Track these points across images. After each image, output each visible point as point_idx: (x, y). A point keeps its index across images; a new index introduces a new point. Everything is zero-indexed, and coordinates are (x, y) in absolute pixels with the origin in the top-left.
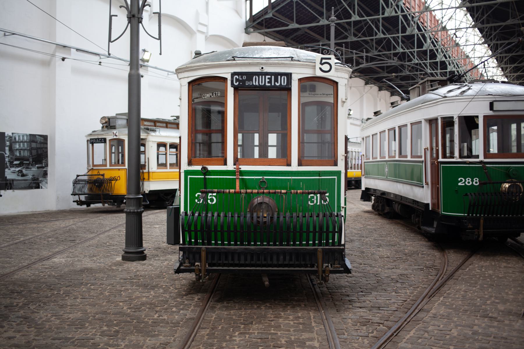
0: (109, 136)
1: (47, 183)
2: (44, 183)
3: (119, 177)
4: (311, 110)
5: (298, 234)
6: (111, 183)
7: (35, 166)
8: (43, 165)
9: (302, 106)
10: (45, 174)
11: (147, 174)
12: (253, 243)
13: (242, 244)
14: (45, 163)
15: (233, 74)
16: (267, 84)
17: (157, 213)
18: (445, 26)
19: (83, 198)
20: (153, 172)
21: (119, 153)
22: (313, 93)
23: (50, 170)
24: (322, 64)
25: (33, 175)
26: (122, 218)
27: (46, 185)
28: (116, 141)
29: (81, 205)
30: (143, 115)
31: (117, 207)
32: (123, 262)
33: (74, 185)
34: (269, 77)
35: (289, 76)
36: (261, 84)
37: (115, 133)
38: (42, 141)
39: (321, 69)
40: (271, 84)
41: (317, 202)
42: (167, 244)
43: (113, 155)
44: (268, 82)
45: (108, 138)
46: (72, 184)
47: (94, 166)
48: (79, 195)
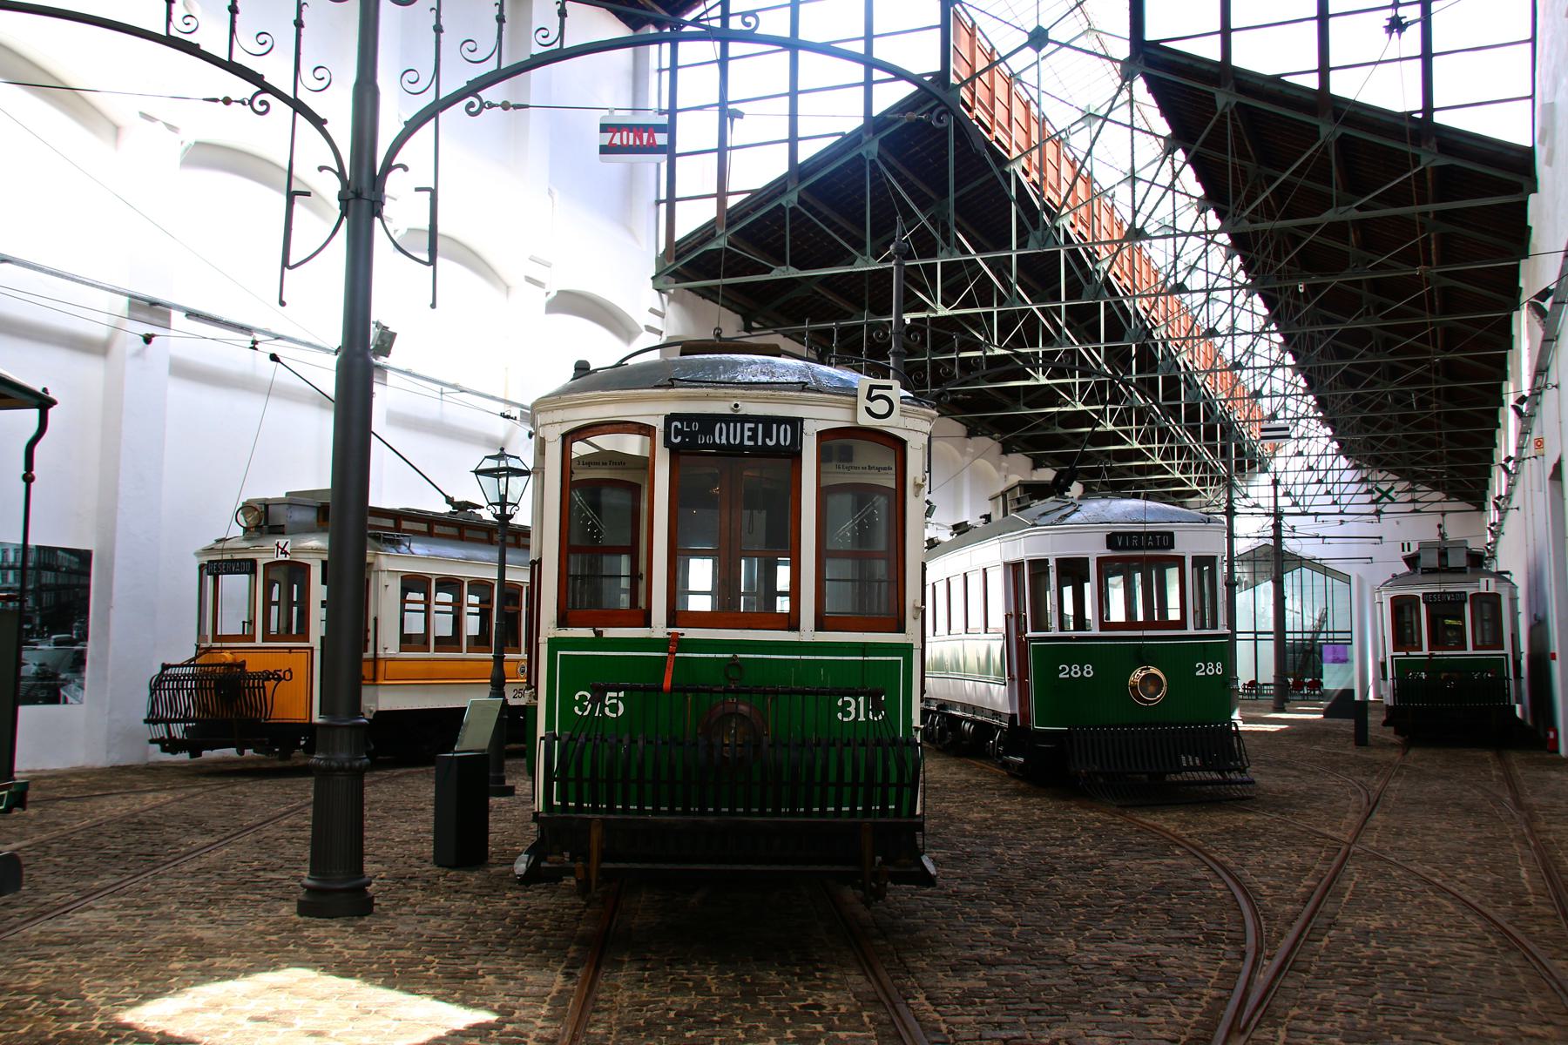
0: (269, 551)
1: (81, 687)
2: (73, 687)
3: (290, 670)
4: (844, 502)
5: (817, 790)
6: (264, 687)
7: (49, 637)
8: (74, 637)
9: (823, 493)
10: (79, 662)
11: (371, 664)
12: (711, 809)
13: (686, 812)
14: (79, 629)
15: (670, 419)
16: (747, 443)
17: (400, 776)
18: (1182, 283)
19: (178, 730)
20: (386, 660)
21: (291, 604)
22: (846, 464)
23: (91, 648)
24: (870, 398)
25: (40, 665)
26: (303, 791)
27: (80, 693)
28: (283, 568)
29: (174, 753)
30: (374, 502)
31: (281, 759)
32: (301, 919)
33: (151, 695)
34: (752, 425)
35: (796, 424)
36: (732, 442)
37: (282, 545)
38: (75, 567)
39: (868, 410)
40: (756, 442)
41: (857, 715)
42: (435, 867)
43: (274, 609)
44: (750, 438)
45: (263, 559)
46: (148, 692)
47: (216, 638)
48: (168, 722)
